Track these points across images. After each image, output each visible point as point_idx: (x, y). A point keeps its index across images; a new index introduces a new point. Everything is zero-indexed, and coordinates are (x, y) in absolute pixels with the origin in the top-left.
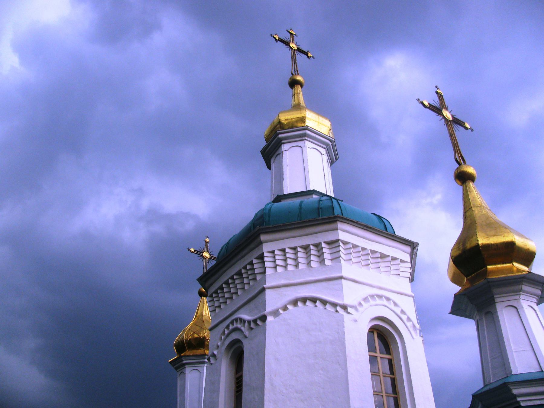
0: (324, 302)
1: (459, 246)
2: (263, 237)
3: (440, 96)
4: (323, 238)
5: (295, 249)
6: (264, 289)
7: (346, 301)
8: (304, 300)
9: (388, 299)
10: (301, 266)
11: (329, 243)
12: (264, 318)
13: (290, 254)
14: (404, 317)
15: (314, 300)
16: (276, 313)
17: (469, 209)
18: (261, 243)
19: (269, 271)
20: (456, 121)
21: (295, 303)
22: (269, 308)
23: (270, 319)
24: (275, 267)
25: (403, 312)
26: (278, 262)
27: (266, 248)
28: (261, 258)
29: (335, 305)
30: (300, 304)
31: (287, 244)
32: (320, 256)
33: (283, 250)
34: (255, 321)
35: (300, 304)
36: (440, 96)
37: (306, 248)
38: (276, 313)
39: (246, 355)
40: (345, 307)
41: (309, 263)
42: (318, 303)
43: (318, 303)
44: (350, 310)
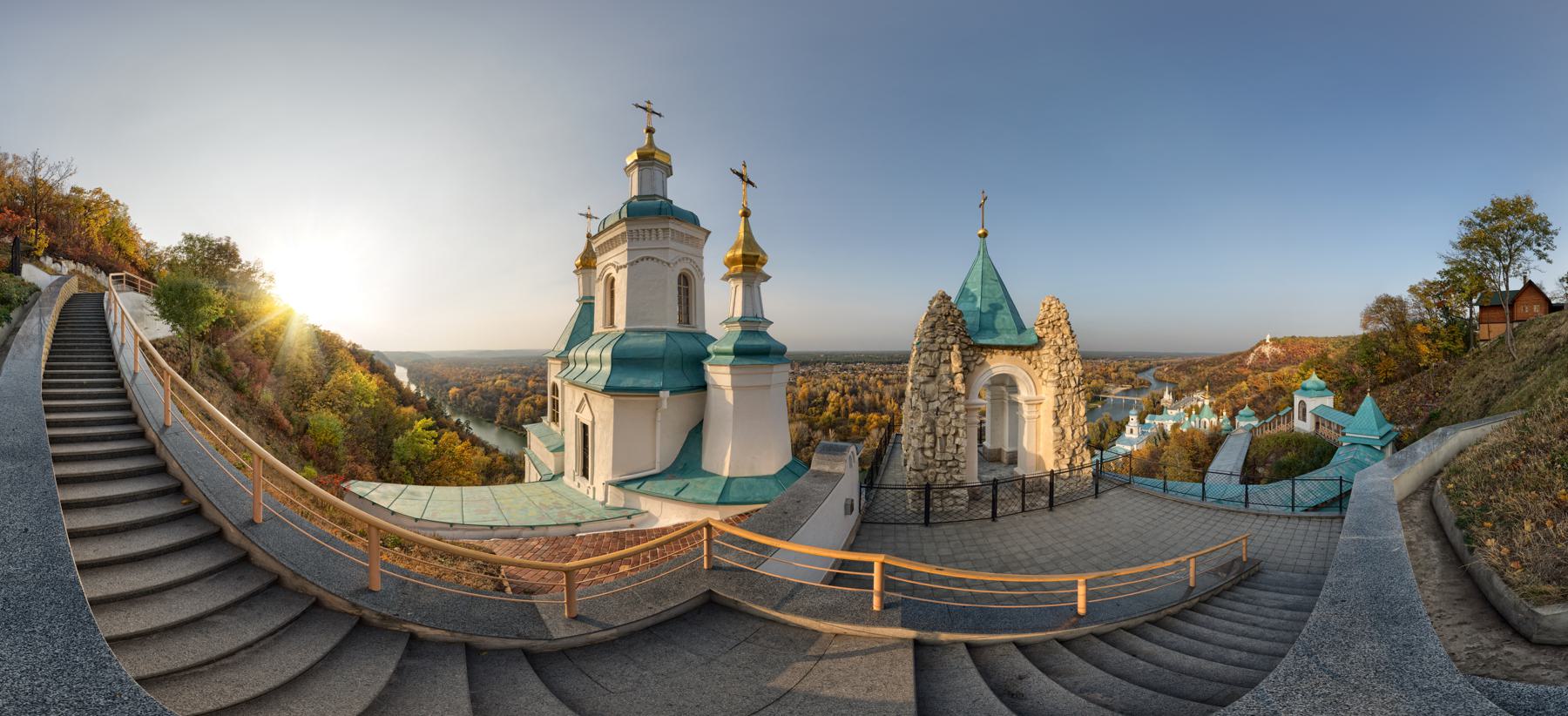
4: (660, 226)
21: (642, 259)
37: (650, 230)
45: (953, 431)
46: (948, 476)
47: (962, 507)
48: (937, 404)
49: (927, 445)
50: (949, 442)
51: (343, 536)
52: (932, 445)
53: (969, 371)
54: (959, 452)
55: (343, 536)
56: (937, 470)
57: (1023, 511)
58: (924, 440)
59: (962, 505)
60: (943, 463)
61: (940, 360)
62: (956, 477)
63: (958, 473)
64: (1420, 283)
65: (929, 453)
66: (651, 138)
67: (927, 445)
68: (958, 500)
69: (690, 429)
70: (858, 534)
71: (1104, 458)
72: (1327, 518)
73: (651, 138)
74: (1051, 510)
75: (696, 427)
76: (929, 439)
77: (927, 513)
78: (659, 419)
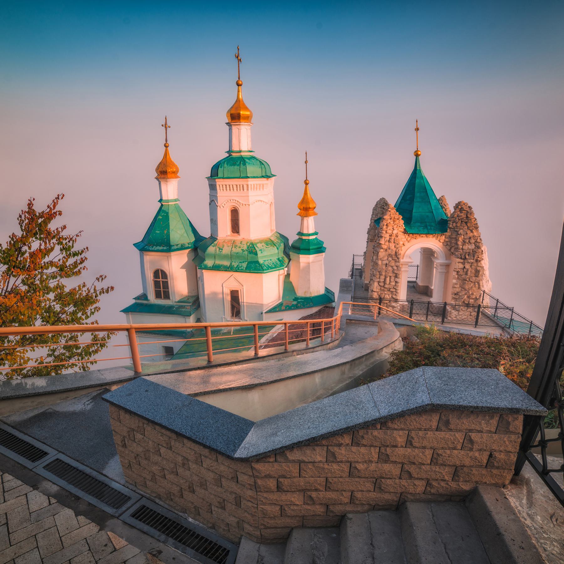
14: (236, 202)
33: (226, 185)
50: (392, 280)
63: (396, 295)
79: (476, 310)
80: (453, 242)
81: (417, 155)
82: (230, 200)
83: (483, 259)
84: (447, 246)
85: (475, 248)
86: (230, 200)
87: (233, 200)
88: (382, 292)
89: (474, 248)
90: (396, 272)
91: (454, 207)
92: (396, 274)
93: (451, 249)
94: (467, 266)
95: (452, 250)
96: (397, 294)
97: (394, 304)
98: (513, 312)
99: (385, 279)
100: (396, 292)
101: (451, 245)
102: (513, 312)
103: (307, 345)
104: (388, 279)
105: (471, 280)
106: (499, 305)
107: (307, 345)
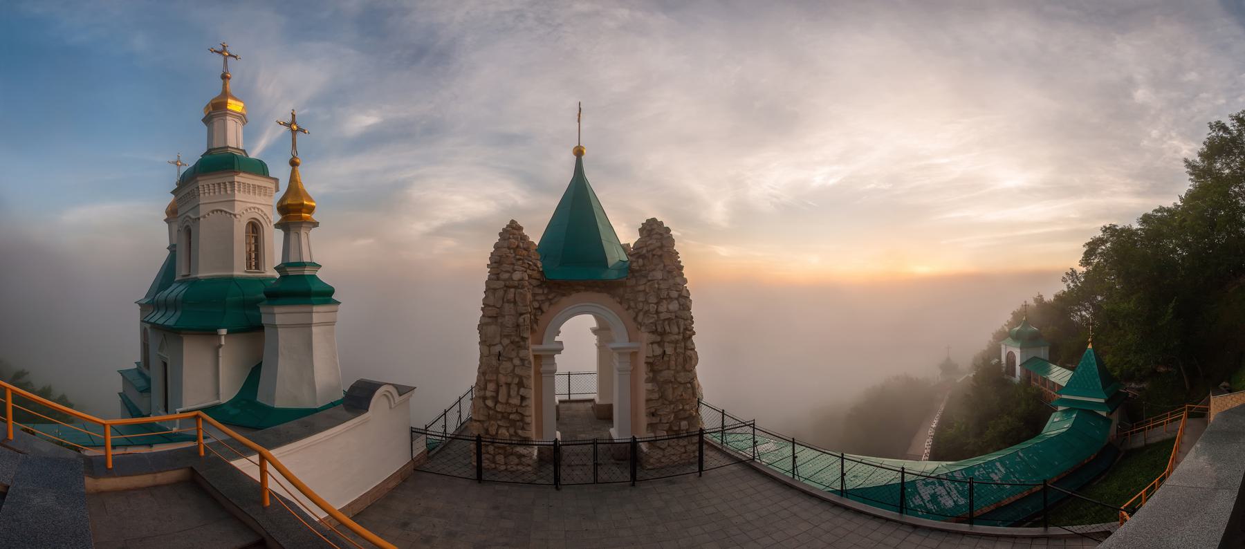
0: (226, 212)
1: (1069, 285)
2: (198, 178)
3: (294, 116)
4: (227, 180)
5: (213, 184)
6: (199, 205)
7: (236, 212)
8: (217, 211)
9: (258, 209)
10: (217, 194)
11: (229, 182)
12: (199, 219)
13: (211, 187)
14: (265, 217)
15: (221, 211)
16: (204, 217)
17: (489, 545)
18: (197, 181)
19: (201, 195)
20: (299, 129)
21: (213, 212)
22: (201, 214)
23: (201, 219)
24: (204, 193)
25: (265, 214)
26: (206, 191)
27: (200, 184)
28: (198, 188)
29: (231, 214)
30: (215, 212)
31: (210, 182)
32: (226, 188)
33: (225, 183)
34: (195, 219)
35: (215, 212)
36: (294, 116)
37: (219, 184)
38: (204, 217)
39: (192, 232)
40: (235, 215)
41: (220, 192)
42: (223, 213)
43: (223, 213)
44: (237, 216)
45: (516, 380)
46: (512, 431)
47: (529, 468)
48: (498, 348)
49: (488, 394)
50: (513, 393)
51: (213, 213)
52: (494, 394)
53: (542, 312)
54: (523, 405)
55: (213, 213)
56: (499, 422)
57: (596, 482)
58: (485, 389)
59: (529, 465)
60: (505, 416)
61: (503, 299)
62: (520, 432)
63: (523, 429)
64: (1155, 210)
65: (490, 403)
66: (225, 85)
67: (488, 394)
68: (523, 459)
69: (253, 366)
70: (405, 480)
71: (725, 424)
72: (1024, 537)
73: (225, 85)
74: (633, 485)
75: (257, 366)
76: (491, 386)
77: (479, 468)
78: (221, 354)
79: (696, 439)
80: (639, 299)
81: (579, 152)
82: (247, 210)
83: (694, 333)
84: (630, 311)
85: (680, 309)
86: (247, 210)
87: (250, 209)
88: (492, 422)
89: (677, 309)
90: (518, 371)
91: (639, 229)
92: (521, 377)
93: (637, 315)
94: (669, 350)
95: (640, 318)
96: (525, 426)
97: (521, 450)
98: (754, 428)
99: (497, 392)
100: (522, 420)
101: (637, 308)
102: (754, 428)
103: (502, 403)
104: (503, 391)
105: (679, 380)
106: (728, 422)
107: (502, 403)
